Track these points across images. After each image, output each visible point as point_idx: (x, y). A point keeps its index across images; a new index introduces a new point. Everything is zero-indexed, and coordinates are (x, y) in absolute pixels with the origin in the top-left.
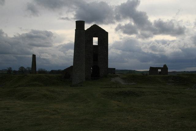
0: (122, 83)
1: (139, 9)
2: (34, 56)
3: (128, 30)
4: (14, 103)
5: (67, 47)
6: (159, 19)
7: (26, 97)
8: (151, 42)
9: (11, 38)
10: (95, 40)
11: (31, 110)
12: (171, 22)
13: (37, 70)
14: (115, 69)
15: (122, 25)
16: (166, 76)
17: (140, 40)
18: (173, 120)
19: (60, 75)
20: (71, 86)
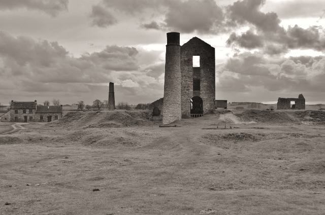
0: (236, 121)
1: (263, 10)
2: (112, 85)
3: (248, 41)
4: (78, 149)
5: (155, 71)
6: (296, 25)
7: (95, 142)
8: (283, 62)
9: (78, 59)
10: (196, 61)
11: (95, 159)
12: (314, 28)
13: (116, 104)
14: (226, 101)
15: (245, 34)
16: (303, 110)
17: (266, 57)
18: (287, 174)
19: (147, 110)
20: (160, 127)
